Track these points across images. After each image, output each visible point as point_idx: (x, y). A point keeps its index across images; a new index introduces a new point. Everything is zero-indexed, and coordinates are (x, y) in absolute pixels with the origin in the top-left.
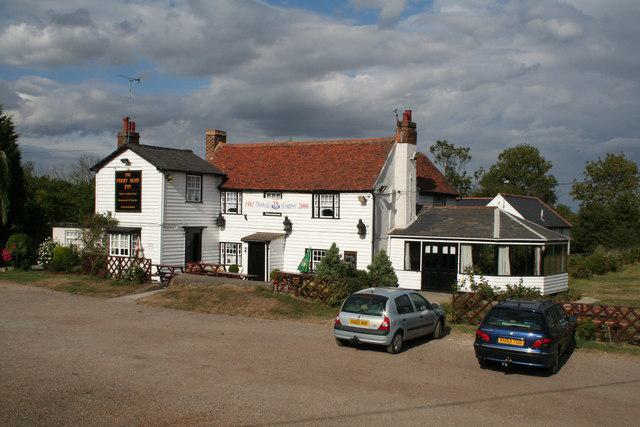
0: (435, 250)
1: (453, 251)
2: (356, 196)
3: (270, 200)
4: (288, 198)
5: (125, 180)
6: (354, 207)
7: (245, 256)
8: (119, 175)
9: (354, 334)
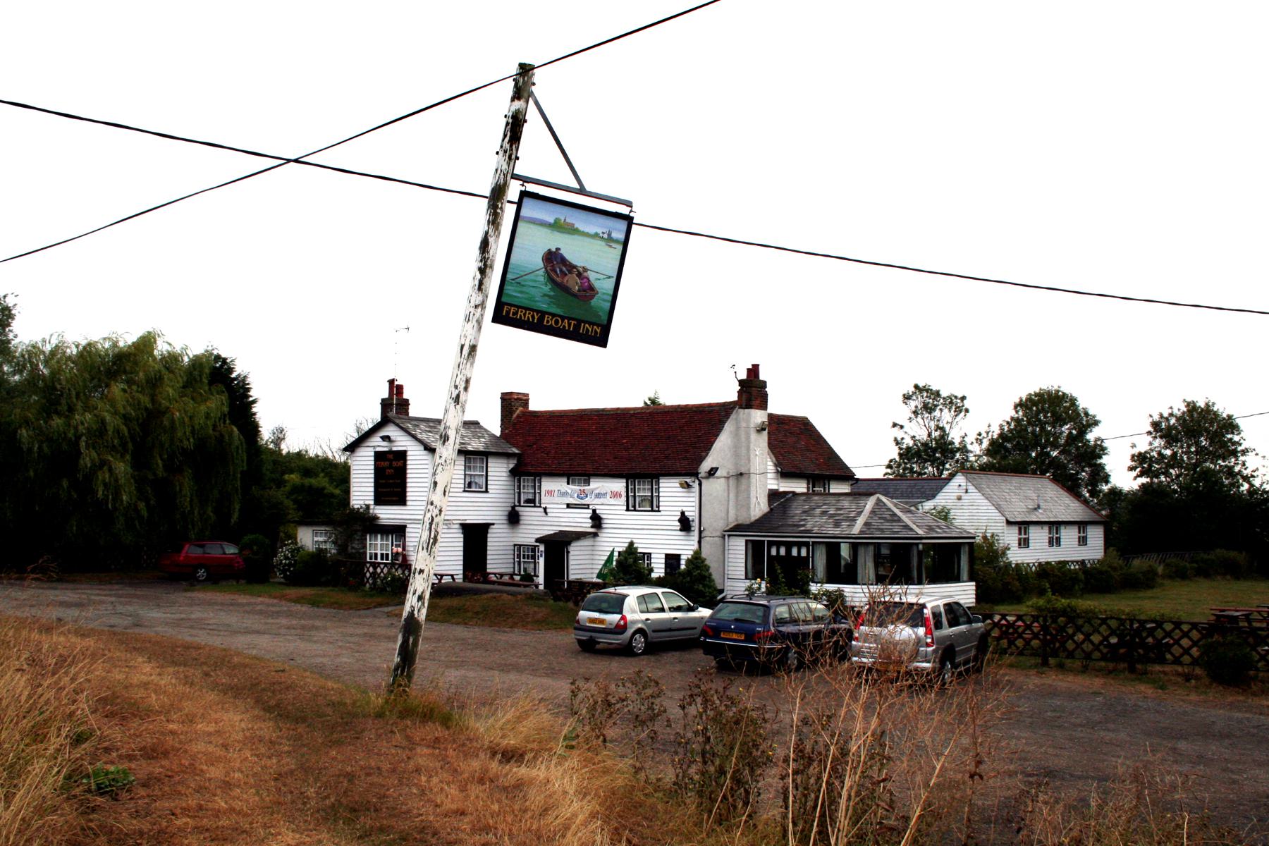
0: (783, 551)
1: (804, 553)
2: (619, 485)
3: (574, 488)
4: (597, 485)
5: (387, 464)
7: (542, 561)
8: (379, 456)
9: (589, 634)
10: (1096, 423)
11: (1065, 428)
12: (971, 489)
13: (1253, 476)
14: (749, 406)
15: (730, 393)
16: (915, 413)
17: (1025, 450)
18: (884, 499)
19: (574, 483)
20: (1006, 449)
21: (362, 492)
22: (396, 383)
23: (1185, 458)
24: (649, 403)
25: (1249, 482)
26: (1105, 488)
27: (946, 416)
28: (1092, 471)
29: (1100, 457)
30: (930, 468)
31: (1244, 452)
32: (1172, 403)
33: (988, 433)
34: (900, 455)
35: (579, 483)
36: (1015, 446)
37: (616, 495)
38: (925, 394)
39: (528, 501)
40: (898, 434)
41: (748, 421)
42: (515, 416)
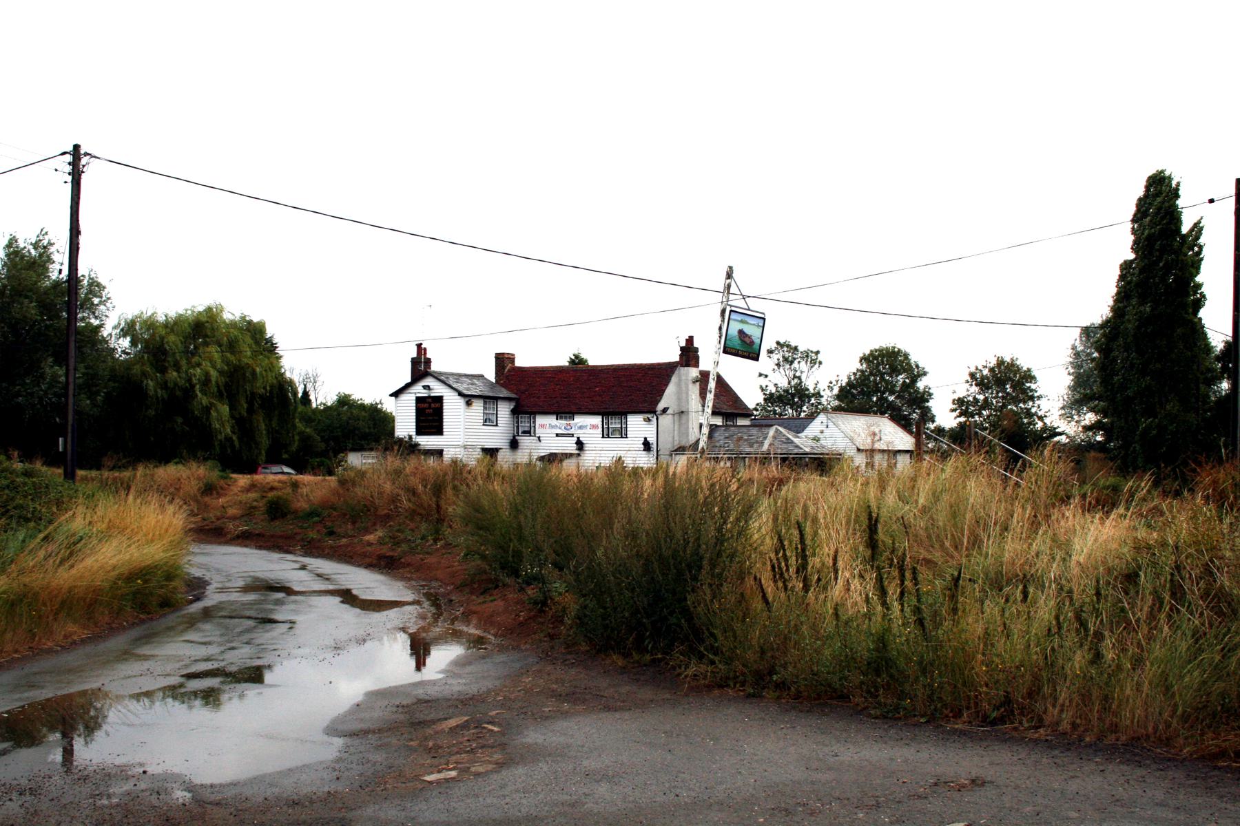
2: (597, 420)
3: (563, 422)
4: (579, 420)
6: (638, 426)
8: (419, 400)
10: (925, 374)
11: (901, 378)
12: (831, 424)
13: (1046, 416)
14: (688, 365)
15: (675, 357)
16: (778, 365)
17: (869, 395)
18: (780, 428)
19: (561, 418)
20: (853, 395)
21: (405, 426)
22: (423, 346)
23: (994, 401)
24: (573, 357)
25: (1042, 421)
26: (932, 426)
27: (801, 366)
28: (921, 412)
29: (928, 401)
30: (790, 411)
31: (1039, 398)
32: (984, 359)
33: (837, 381)
34: (765, 399)
35: (566, 418)
36: (859, 392)
37: (594, 427)
38: (785, 349)
39: (524, 432)
40: (763, 382)
41: (687, 375)
42: (506, 370)
